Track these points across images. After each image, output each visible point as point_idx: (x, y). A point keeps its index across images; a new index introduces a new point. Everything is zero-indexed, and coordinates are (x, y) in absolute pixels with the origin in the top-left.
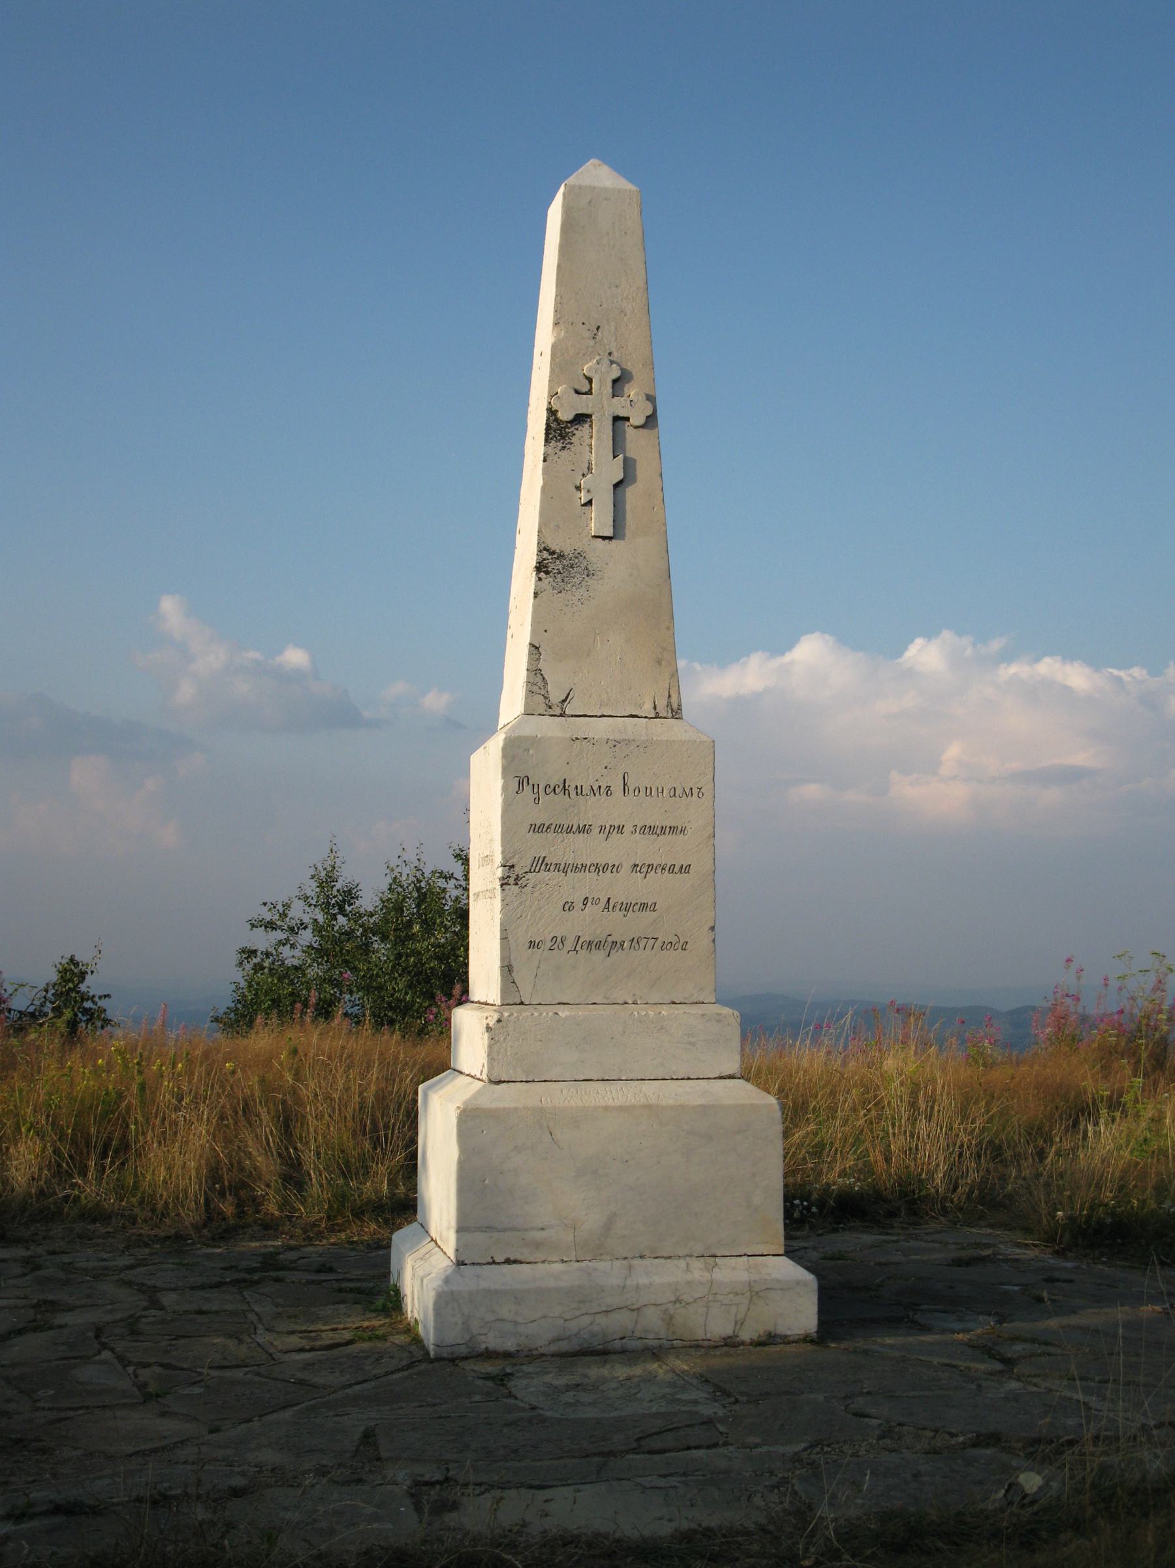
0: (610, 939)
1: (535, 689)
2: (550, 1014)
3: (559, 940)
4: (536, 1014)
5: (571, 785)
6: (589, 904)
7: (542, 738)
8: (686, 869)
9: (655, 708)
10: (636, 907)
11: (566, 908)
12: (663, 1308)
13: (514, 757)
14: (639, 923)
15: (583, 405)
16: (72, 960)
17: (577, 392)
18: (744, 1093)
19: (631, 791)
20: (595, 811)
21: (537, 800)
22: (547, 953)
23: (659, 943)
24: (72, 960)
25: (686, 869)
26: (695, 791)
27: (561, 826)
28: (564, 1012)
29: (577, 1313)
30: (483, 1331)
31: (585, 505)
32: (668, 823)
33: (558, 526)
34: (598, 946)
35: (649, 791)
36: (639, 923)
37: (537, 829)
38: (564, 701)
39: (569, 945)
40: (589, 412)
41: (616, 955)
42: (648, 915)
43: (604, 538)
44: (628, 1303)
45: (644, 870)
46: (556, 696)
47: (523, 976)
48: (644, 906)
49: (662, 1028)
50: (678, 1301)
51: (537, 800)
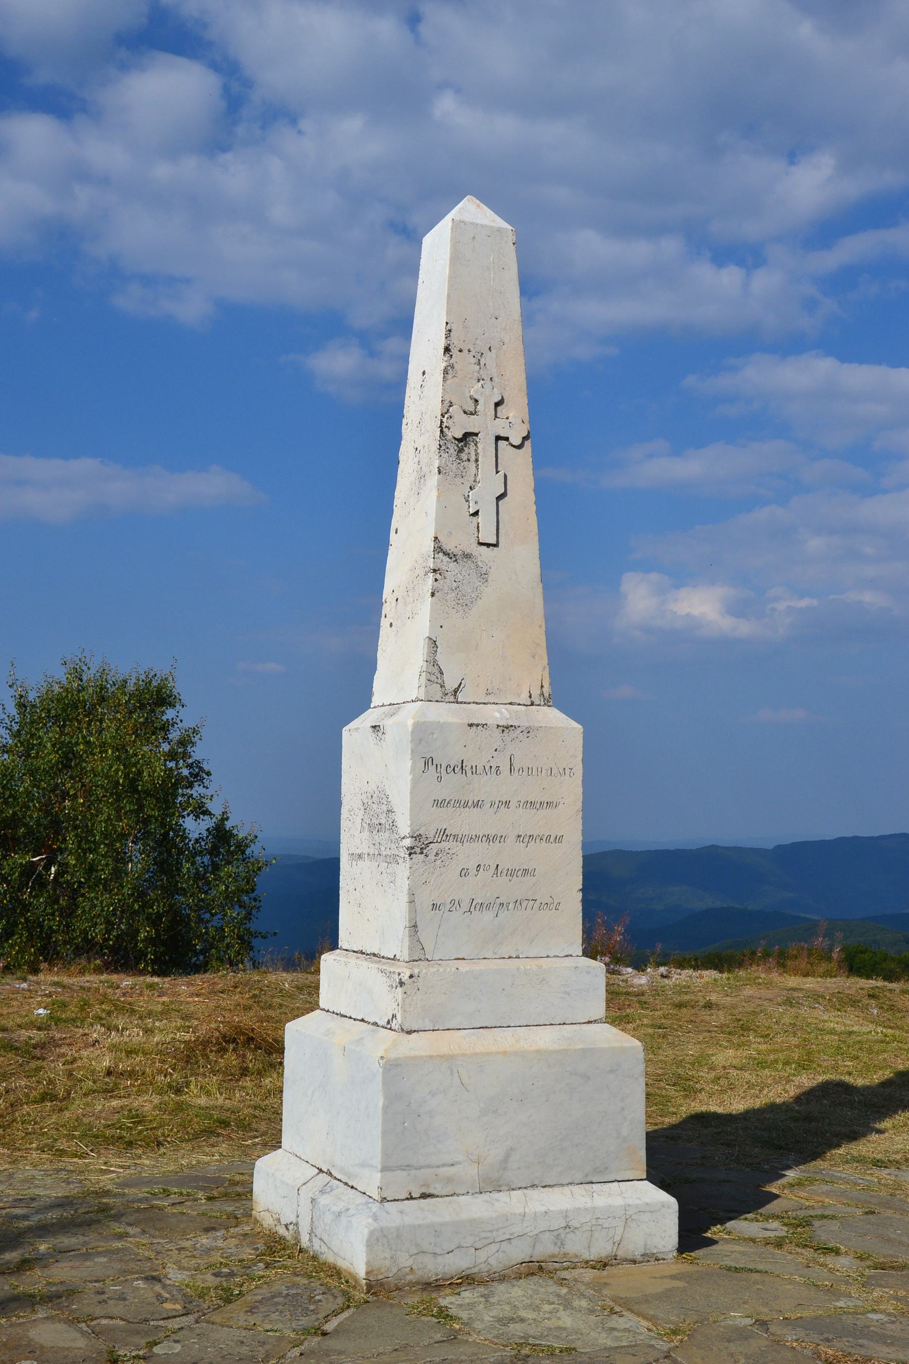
0: (498, 901)
1: (433, 678)
2: (454, 969)
3: (456, 902)
4: (441, 970)
6: (481, 870)
7: (444, 723)
8: (559, 839)
9: (530, 697)
10: (520, 873)
11: (463, 874)
12: (556, 1233)
13: (421, 741)
15: (471, 424)
16: (156, 699)
17: (465, 412)
18: (611, 1037)
19: (516, 771)
20: (486, 788)
21: (440, 779)
22: (447, 913)
24: (156, 699)
25: (559, 839)
26: (568, 771)
28: (464, 967)
29: (486, 1242)
33: (451, 533)
34: (488, 907)
37: (438, 803)
39: (465, 906)
40: (476, 431)
41: (503, 914)
43: (488, 545)
45: (526, 840)
46: (451, 685)
47: (425, 936)
50: (567, 1227)
51: (440, 779)
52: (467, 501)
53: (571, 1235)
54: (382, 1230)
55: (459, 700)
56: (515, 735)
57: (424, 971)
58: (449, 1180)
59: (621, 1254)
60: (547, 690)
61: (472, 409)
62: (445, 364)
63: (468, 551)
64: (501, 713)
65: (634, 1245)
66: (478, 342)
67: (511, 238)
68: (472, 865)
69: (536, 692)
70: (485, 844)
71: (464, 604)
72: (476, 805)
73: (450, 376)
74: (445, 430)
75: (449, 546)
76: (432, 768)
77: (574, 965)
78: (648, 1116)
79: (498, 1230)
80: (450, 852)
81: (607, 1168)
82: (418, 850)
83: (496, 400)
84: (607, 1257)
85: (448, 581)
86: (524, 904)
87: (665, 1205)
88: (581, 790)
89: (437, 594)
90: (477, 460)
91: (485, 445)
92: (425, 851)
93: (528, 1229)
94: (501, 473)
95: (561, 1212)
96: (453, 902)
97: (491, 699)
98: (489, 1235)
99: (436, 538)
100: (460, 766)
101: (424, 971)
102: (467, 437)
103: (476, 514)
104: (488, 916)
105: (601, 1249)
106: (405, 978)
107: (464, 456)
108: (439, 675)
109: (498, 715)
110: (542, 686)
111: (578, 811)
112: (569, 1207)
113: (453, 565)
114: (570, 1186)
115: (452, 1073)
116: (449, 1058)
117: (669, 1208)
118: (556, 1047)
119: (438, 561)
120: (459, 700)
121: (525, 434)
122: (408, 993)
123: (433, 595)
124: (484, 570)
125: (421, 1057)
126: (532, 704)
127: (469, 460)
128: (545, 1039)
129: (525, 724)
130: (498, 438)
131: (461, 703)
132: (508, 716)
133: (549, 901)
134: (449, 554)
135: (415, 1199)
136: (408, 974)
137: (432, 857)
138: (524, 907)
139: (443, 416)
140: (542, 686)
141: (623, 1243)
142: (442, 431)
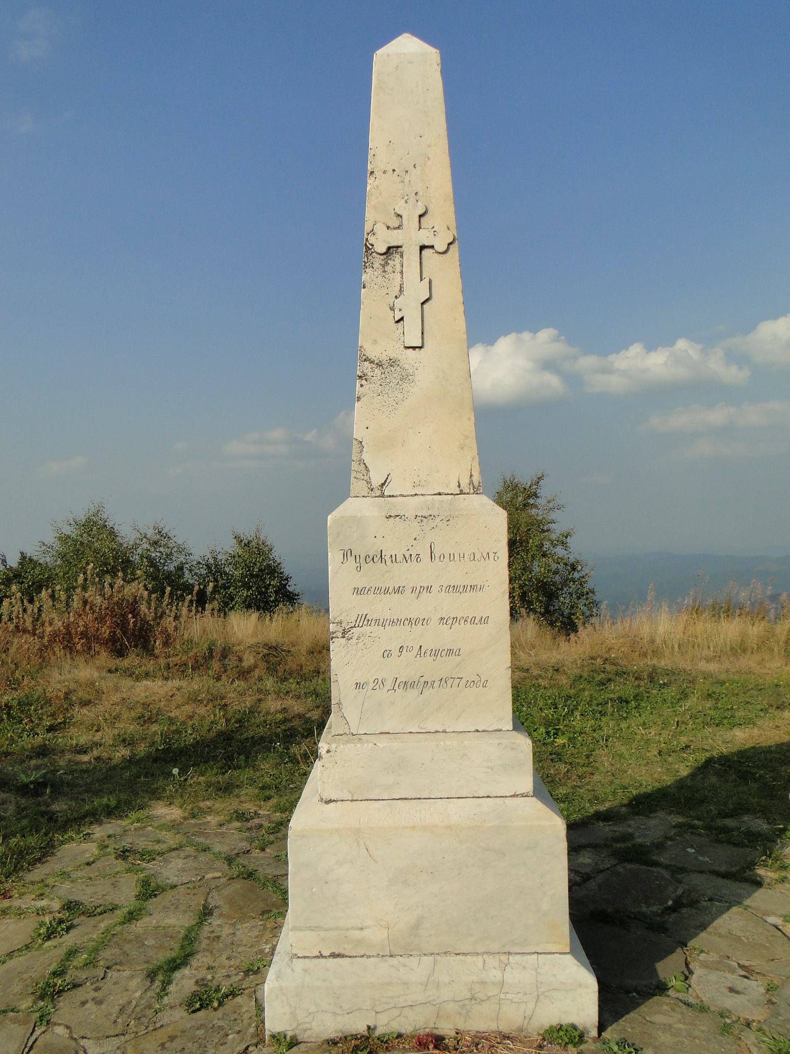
0: (422, 680)
3: (380, 682)
5: (387, 555)
8: (484, 620)
9: (459, 486)
11: (386, 655)
12: (461, 1003)
14: (445, 667)
15: (395, 238)
20: (405, 574)
23: (463, 682)
25: (484, 620)
26: (492, 555)
27: (380, 589)
29: (387, 1007)
30: (307, 1020)
31: (398, 322)
32: (468, 583)
34: (413, 685)
35: (451, 557)
36: (445, 667)
37: (358, 591)
38: (383, 484)
41: (428, 692)
42: (454, 659)
43: (414, 348)
44: (431, 999)
45: (450, 622)
46: (377, 481)
48: (450, 652)
49: (465, 755)
56: (434, 525)
58: (359, 942)
60: (476, 478)
72: (398, 591)
79: (398, 997)
82: (340, 635)
83: (421, 212)
86: (450, 682)
90: (402, 272)
91: (411, 254)
94: (427, 280)
100: (379, 556)
107: (388, 268)
110: (471, 476)
117: (586, 987)
126: (461, 493)
128: (458, 812)
130: (422, 248)
133: (476, 679)
135: (325, 957)
140: (471, 476)
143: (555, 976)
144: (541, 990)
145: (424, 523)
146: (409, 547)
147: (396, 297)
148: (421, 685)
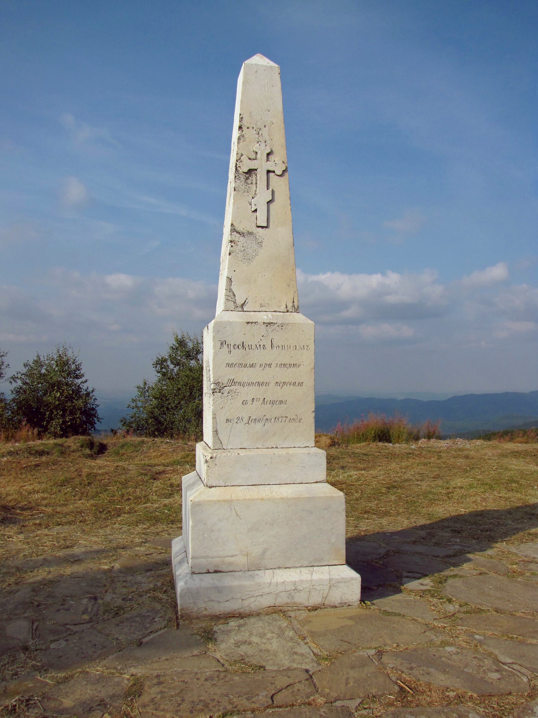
2: (236, 454)
3: (240, 419)
4: (229, 454)
6: (255, 401)
8: (301, 384)
9: (287, 307)
11: (244, 403)
15: (253, 165)
17: (250, 159)
18: (328, 490)
20: (258, 357)
21: (230, 352)
22: (235, 424)
23: (288, 419)
25: (301, 384)
27: (241, 364)
28: (243, 453)
29: (248, 596)
31: (253, 212)
33: (241, 221)
34: (259, 421)
36: (278, 410)
37: (229, 365)
39: (246, 419)
40: (256, 168)
41: (268, 424)
42: (283, 406)
43: (262, 227)
45: (281, 385)
46: (240, 302)
48: (281, 402)
50: (296, 589)
51: (230, 352)
52: (251, 205)
53: (298, 594)
54: (188, 589)
55: (245, 310)
56: (274, 328)
57: (219, 455)
58: (231, 564)
59: (327, 602)
61: (254, 157)
62: (239, 135)
63: (251, 231)
64: (267, 316)
65: (335, 597)
66: (258, 123)
67: (278, 71)
68: (249, 398)
69: (290, 305)
70: (257, 387)
71: (248, 259)
72: (252, 366)
73: (241, 141)
74: (238, 168)
75: (239, 228)
76: (225, 346)
77: (307, 452)
78: (347, 532)
80: (236, 391)
81: (322, 559)
82: (218, 390)
84: (319, 604)
85: (239, 247)
86: (280, 419)
87: (353, 577)
88: (313, 357)
89: (232, 254)
90: (256, 183)
91: (261, 176)
92: (222, 391)
93: (273, 591)
94: (271, 189)
95: (292, 582)
96: (238, 418)
97: (263, 309)
98: (250, 593)
99: (232, 224)
100: (242, 345)
101: (219, 455)
102: (250, 172)
103: (256, 211)
104: (259, 425)
105: (316, 600)
106: (208, 458)
107: (249, 181)
108: (233, 297)
109: (265, 317)
110: (294, 302)
111: (312, 369)
112: (297, 580)
113: (242, 238)
114: (301, 568)
115: (231, 509)
116: (230, 502)
118: (293, 496)
119: (234, 236)
120: (245, 310)
121: (284, 169)
122: (210, 466)
123: (230, 254)
124: (260, 240)
125: (213, 501)
126: (288, 311)
127: (252, 183)
128: (287, 491)
129: (280, 322)
130: (268, 172)
131: (246, 311)
132: (271, 318)
133: (295, 417)
134: (239, 233)
136: (210, 457)
137: (226, 394)
138: (280, 420)
139: (237, 161)
140: (294, 302)
141: (328, 598)
142: (236, 169)
143: (339, 575)
144: (332, 583)
145: (268, 327)
146: (259, 340)
147: (253, 198)
148: (264, 421)
